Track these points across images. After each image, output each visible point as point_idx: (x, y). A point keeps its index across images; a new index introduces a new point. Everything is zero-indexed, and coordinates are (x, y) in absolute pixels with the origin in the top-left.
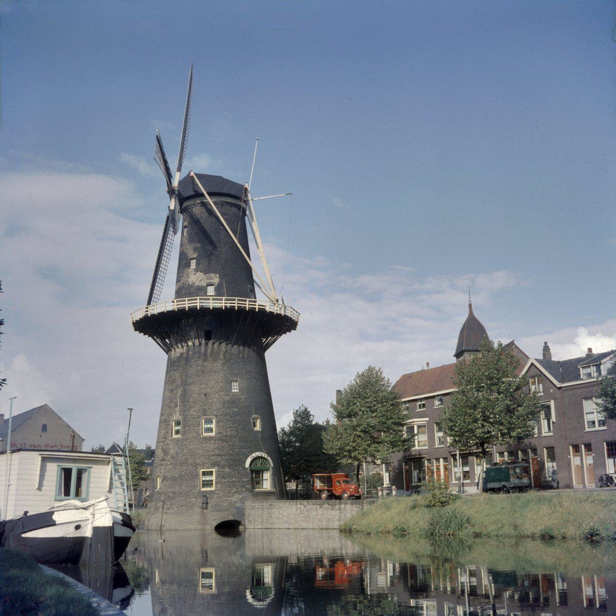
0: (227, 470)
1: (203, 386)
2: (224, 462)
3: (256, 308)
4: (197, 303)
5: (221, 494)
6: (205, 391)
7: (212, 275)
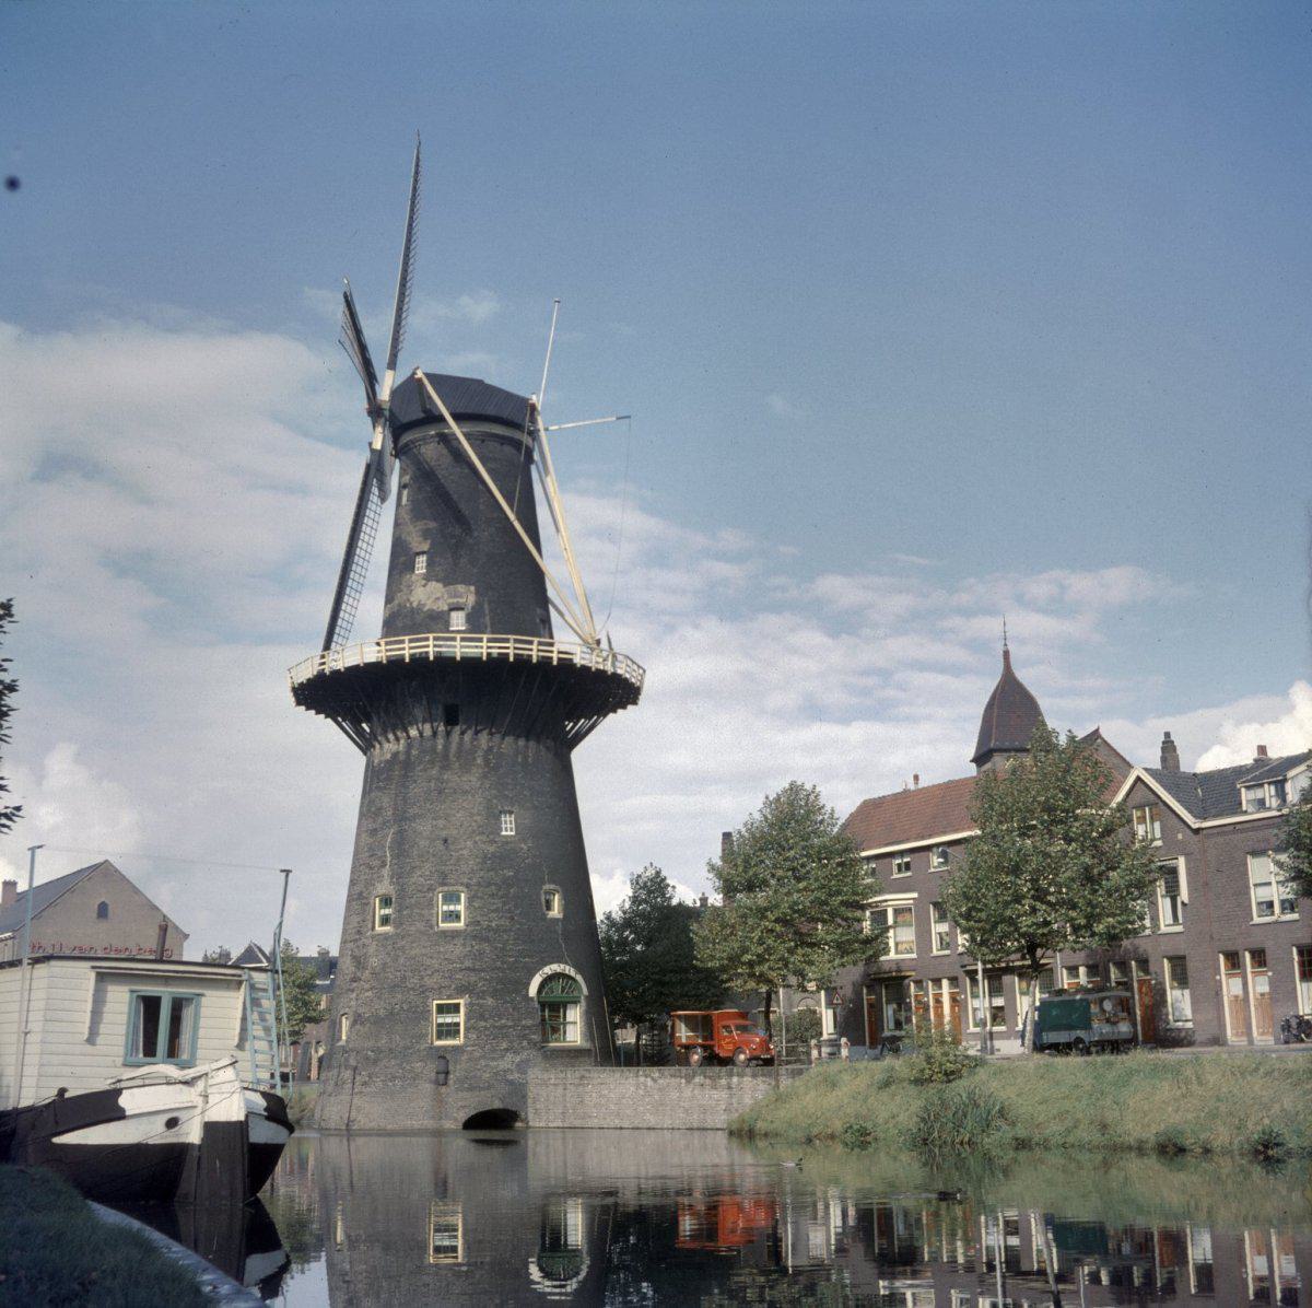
0: (490, 1001)
1: (441, 823)
4: (428, 646)
5: (477, 1054)
6: (444, 834)
7: (461, 588)
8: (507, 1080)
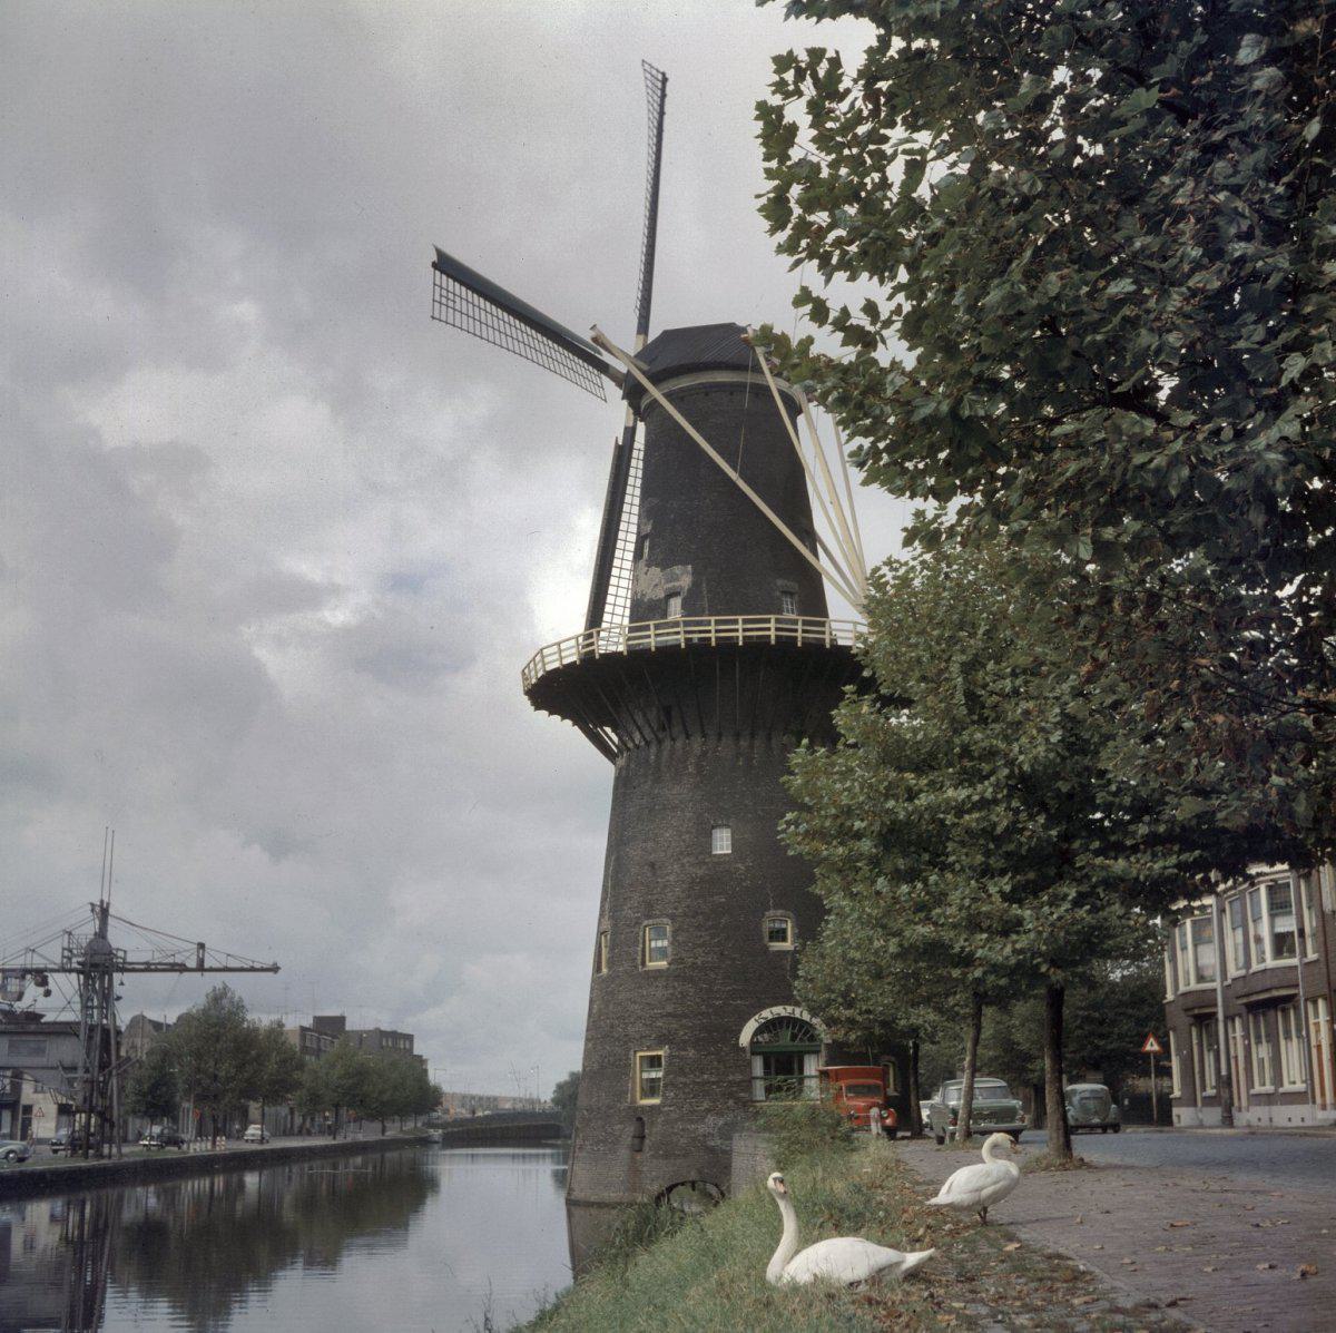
0: (691, 1053)
1: (650, 844)
2: (686, 1034)
3: (796, 638)
4: (769, 629)
5: (673, 1115)
7: (677, 569)
8: (707, 1148)
